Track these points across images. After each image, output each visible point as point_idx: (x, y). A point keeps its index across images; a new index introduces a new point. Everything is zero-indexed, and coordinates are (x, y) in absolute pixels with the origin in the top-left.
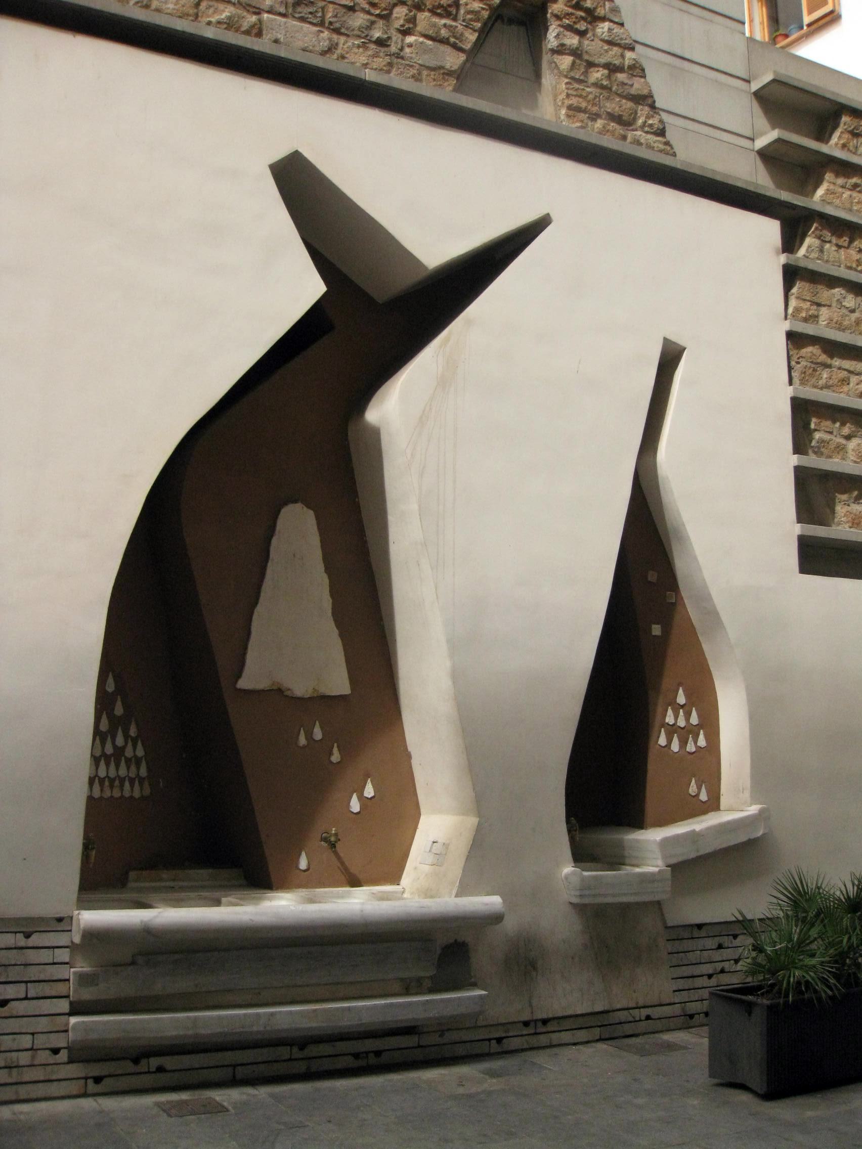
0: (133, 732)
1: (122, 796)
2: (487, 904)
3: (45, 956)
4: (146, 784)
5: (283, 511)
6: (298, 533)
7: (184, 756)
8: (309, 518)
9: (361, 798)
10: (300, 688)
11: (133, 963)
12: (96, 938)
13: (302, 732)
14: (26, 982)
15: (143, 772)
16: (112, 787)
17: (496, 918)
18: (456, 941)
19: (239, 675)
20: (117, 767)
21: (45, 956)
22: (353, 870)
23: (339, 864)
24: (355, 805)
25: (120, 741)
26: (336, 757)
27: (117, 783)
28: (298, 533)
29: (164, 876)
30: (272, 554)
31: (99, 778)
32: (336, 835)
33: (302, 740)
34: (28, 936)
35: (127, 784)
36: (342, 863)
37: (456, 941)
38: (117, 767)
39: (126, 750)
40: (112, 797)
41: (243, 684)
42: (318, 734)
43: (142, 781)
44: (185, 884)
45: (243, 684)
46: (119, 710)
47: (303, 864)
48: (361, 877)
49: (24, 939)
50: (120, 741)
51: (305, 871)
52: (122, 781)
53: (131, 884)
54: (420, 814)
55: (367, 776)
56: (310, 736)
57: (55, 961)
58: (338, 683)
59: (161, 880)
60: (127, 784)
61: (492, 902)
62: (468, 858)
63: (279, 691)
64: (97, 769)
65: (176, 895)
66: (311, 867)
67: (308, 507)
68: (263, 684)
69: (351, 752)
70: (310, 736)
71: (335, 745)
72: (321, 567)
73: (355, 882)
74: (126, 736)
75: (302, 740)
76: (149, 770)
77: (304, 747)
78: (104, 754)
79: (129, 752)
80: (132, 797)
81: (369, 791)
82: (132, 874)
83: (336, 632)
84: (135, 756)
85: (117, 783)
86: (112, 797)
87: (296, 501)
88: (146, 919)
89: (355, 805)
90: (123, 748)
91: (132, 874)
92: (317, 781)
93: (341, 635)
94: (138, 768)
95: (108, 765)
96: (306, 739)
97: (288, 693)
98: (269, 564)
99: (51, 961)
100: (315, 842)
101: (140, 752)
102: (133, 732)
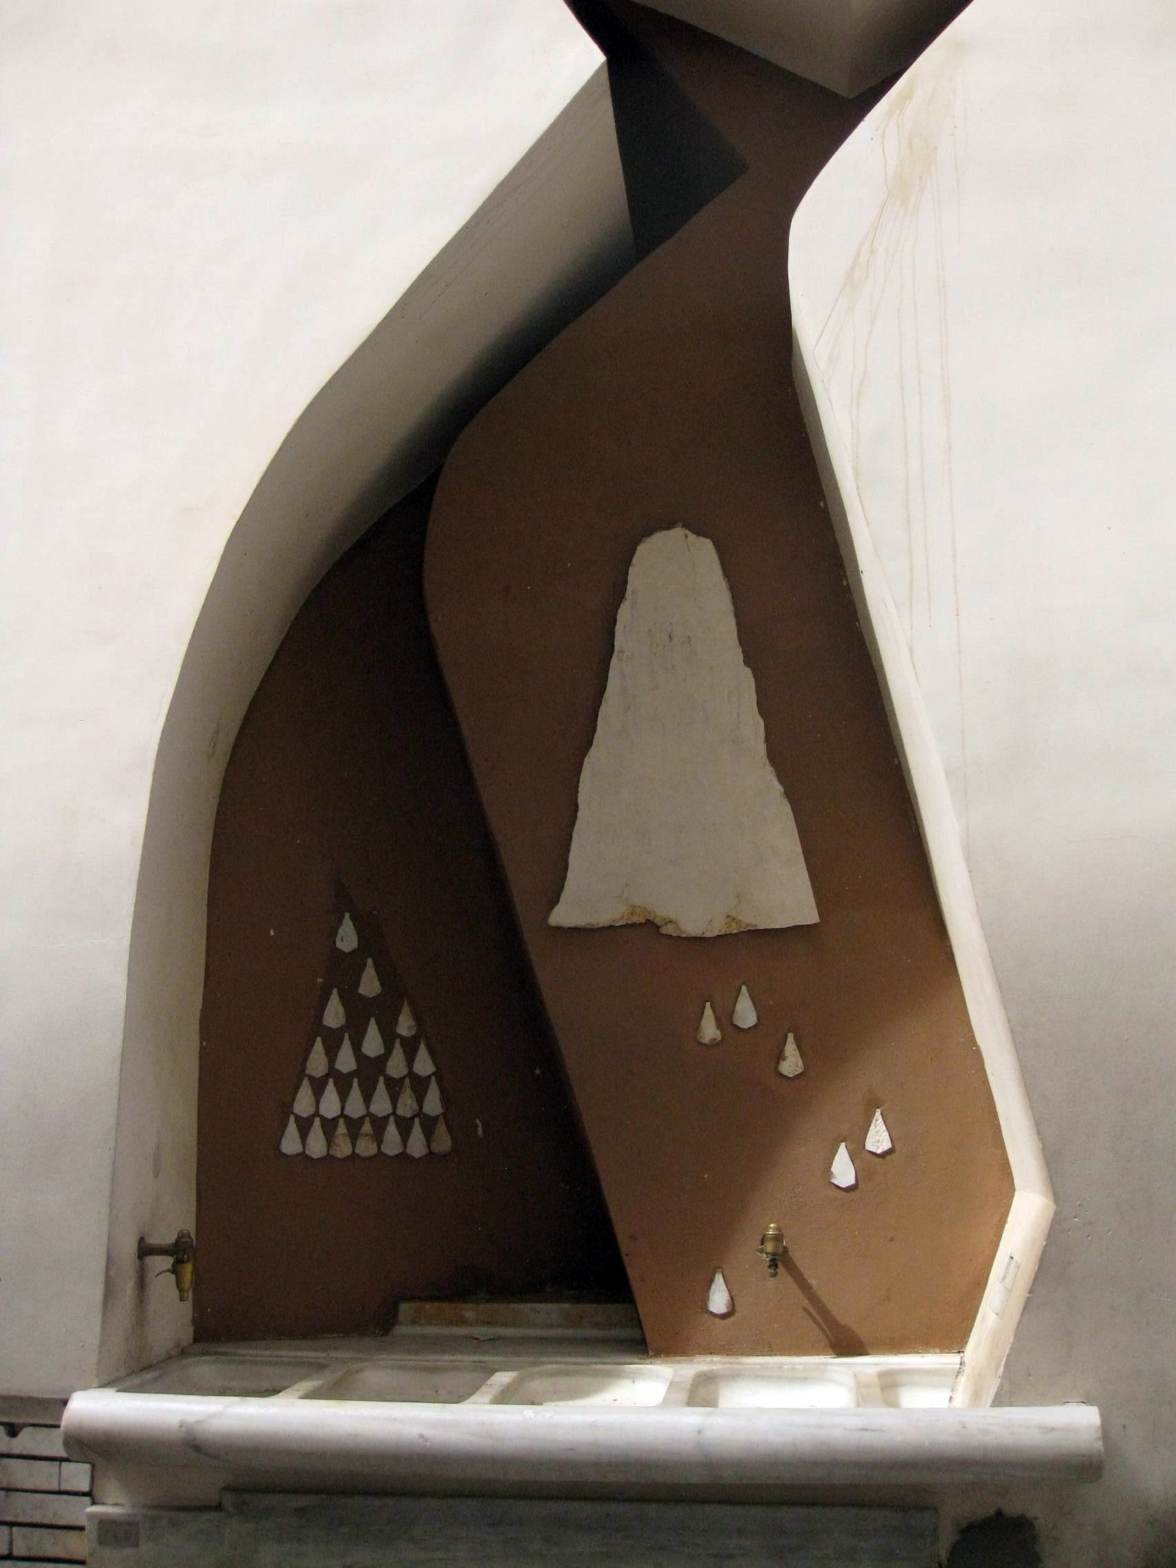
0: (405, 1025)
1: (380, 1154)
2: (1052, 1429)
3: (43, 1475)
4: (441, 1130)
5: (642, 549)
6: (679, 592)
7: (538, 1072)
8: (704, 553)
9: (858, 1153)
10: (696, 916)
11: (219, 1507)
12: (103, 1450)
13: (708, 1011)
14: (11, 1524)
15: (433, 1104)
16: (354, 1136)
17: (1075, 1472)
18: (999, 1514)
19: (554, 901)
20: (367, 1097)
21: (43, 1475)
22: (843, 1318)
23: (806, 1302)
24: (843, 1171)
25: (373, 1044)
26: (792, 1063)
27: (367, 1128)
28: (679, 592)
29: (470, 1314)
30: (621, 638)
31: (322, 1118)
32: (778, 1238)
33: (709, 1030)
34: (13, 1430)
35: (392, 1131)
36: (814, 1299)
37: (999, 1514)
38: (367, 1097)
39: (390, 1063)
40: (354, 1156)
41: (562, 916)
42: (746, 1014)
43: (429, 1125)
44: (510, 1332)
45: (562, 916)
46: (370, 985)
47: (718, 1300)
48: (862, 1332)
49: (6, 1438)
50: (373, 1044)
51: (723, 1316)
52: (379, 1125)
53: (402, 1330)
54: (1012, 1189)
55: (872, 1104)
56: (725, 1020)
57: (63, 1488)
58: (785, 895)
59: (462, 1322)
60: (392, 1131)
61: (1070, 1422)
62: (1027, 1306)
63: (647, 929)
64: (318, 1102)
65: (431, 1359)
66: (738, 1308)
67: (698, 533)
68: (607, 913)
69: (827, 1056)
70: (725, 1020)
71: (791, 1037)
72: (737, 655)
73: (846, 1344)
74: (389, 1036)
75: (709, 1030)
76: (445, 1099)
77: (714, 1044)
78: (332, 1072)
79: (396, 1066)
80: (404, 1157)
81: (878, 1138)
82: (405, 1309)
83: (778, 788)
84: (411, 1074)
85: (367, 1128)
86: (354, 1156)
87: (670, 526)
88: (191, 1419)
89: (843, 1171)
90: (382, 1060)
91: (405, 1309)
92: (749, 1119)
93: (790, 794)
94: (420, 1099)
95: (343, 1095)
96: (719, 1025)
97: (669, 930)
98: (614, 661)
99: (55, 1487)
100: (749, 1255)
101: (424, 1065)
102: (405, 1025)
